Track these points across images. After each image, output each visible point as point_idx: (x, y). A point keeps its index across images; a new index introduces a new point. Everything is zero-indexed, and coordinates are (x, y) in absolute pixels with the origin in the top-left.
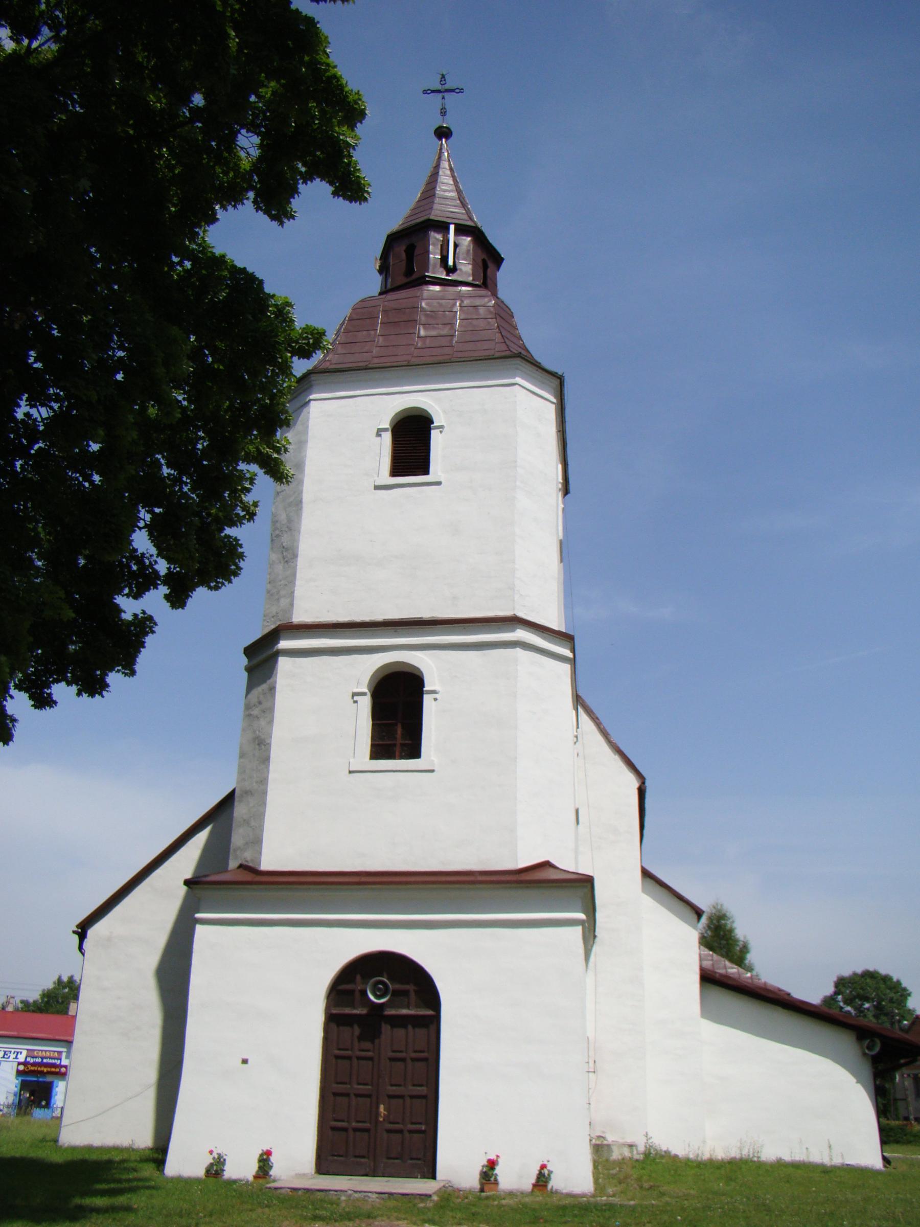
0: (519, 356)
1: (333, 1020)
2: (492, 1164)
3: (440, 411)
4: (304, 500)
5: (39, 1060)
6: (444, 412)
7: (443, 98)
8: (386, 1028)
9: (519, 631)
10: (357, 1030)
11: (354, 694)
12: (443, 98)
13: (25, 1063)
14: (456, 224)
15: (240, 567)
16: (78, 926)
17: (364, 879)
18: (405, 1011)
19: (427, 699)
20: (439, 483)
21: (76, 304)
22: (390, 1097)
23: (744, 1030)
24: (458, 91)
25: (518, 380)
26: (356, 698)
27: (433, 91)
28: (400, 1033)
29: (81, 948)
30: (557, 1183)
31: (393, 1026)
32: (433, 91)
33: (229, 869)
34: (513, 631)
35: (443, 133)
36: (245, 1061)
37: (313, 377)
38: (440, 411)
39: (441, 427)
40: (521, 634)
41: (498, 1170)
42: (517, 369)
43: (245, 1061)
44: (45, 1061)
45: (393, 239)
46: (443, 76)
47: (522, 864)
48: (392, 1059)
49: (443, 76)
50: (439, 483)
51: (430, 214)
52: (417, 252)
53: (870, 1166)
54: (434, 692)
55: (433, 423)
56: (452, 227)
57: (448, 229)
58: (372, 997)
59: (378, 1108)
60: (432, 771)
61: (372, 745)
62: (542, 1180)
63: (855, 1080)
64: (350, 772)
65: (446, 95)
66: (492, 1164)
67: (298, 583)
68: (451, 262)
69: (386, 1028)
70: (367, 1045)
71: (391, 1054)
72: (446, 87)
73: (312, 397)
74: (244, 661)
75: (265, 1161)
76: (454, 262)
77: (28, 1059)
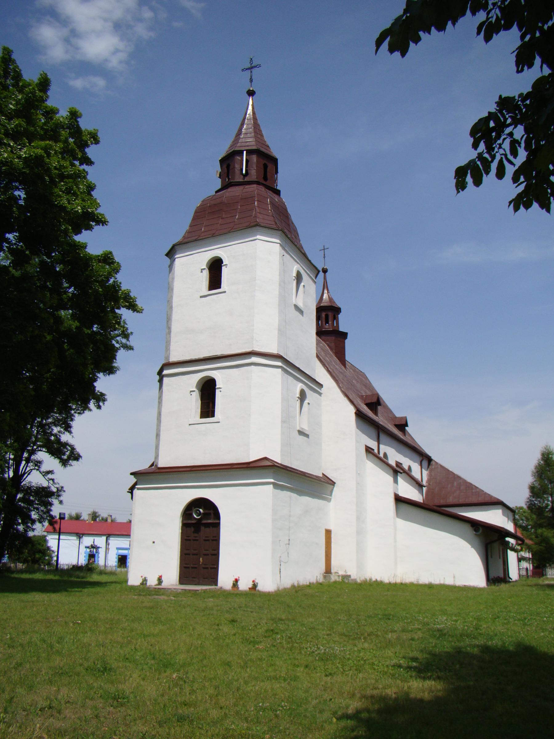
0: (258, 226)
1: (185, 526)
2: (237, 581)
3: (226, 257)
4: (173, 306)
6: (228, 257)
7: (251, 72)
8: (202, 528)
9: (253, 358)
10: (193, 529)
11: (191, 391)
12: (251, 72)
14: (247, 150)
16: (129, 489)
17: (181, 470)
18: (209, 521)
19: (217, 391)
20: (225, 292)
22: (205, 555)
23: (417, 524)
24: (258, 66)
25: (259, 237)
26: (191, 393)
27: (247, 69)
28: (208, 530)
29: (132, 498)
30: (260, 588)
31: (205, 527)
32: (247, 69)
34: (250, 358)
35: (251, 93)
36: (154, 542)
37: (176, 247)
38: (226, 257)
39: (226, 265)
40: (254, 359)
41: (239, 583)
42: (258, 231)
43: (154, 542)
45: (222, 161)
46: (251, 59)
47: (252, 459)
48: (205, 540)
49: (251, 59)
50: (225, 292)
52: (231, 167)
53: (476, 586)
54: (220, 388)
55: (223, 263)
56: (245, 152)
58: (195, 516)
59: (200, 559)
60: (219, 422)
61: (201, 412)
62: (255, 586)
63: (470, 546)
64: (190, 425)
66: (237, 581)
67: (171, 344)
68: (244, 172)
69: (202, 528)
70: (196, 535)
71: (204, 538)
73: (176, 257)
75: (160, 580)
76: (246, 170)
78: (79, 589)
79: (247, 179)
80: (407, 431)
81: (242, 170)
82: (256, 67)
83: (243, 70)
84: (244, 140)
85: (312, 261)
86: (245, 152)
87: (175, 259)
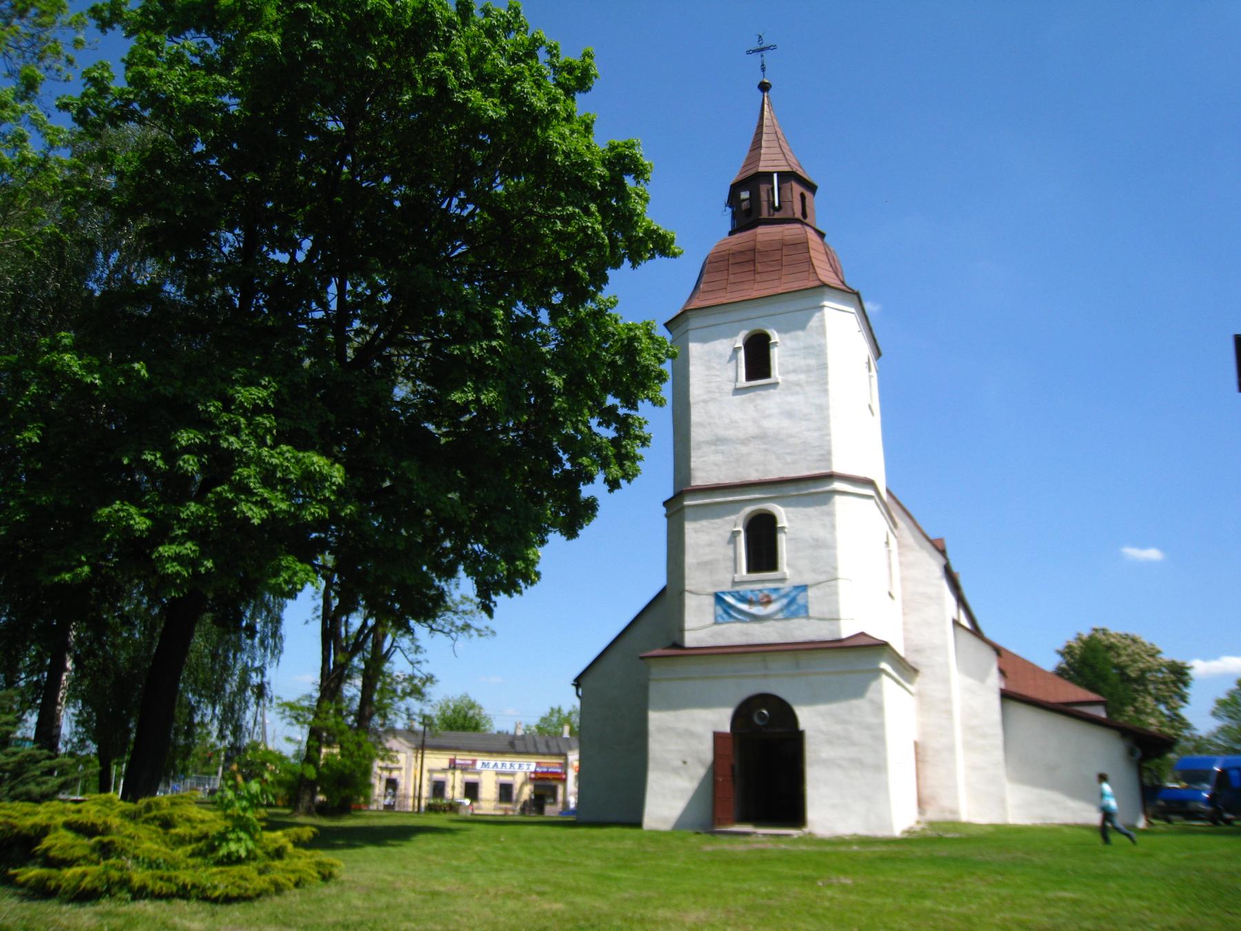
5: (545, 770)
7: (762, 56)
12: (762, 56)
13: (535, 772)
15: (637, 406)
21: (769, 712)
27: (754, 51)
32: (754, 51)
33: (690, 640)
44: (550, 770)
46: (760, 37)
49: (760, 37)
51: (758, 166)
56: (775, 175)
57: (772, 176)
65: (764, 53)
68: (777, 204)
72: (763, 46)
74: (664, 510)
77: (538, 769)
78: (400, 843)
79: (777, 215)
80: (834, 504)
81: (774, 202)
82: (768, 48)
83: (748, 52)
84: (768, 157)
85: (874, 330)
86: (775, 175)
87: (687, 331)
